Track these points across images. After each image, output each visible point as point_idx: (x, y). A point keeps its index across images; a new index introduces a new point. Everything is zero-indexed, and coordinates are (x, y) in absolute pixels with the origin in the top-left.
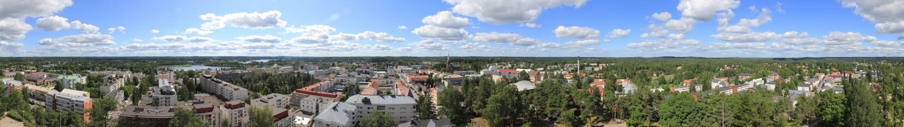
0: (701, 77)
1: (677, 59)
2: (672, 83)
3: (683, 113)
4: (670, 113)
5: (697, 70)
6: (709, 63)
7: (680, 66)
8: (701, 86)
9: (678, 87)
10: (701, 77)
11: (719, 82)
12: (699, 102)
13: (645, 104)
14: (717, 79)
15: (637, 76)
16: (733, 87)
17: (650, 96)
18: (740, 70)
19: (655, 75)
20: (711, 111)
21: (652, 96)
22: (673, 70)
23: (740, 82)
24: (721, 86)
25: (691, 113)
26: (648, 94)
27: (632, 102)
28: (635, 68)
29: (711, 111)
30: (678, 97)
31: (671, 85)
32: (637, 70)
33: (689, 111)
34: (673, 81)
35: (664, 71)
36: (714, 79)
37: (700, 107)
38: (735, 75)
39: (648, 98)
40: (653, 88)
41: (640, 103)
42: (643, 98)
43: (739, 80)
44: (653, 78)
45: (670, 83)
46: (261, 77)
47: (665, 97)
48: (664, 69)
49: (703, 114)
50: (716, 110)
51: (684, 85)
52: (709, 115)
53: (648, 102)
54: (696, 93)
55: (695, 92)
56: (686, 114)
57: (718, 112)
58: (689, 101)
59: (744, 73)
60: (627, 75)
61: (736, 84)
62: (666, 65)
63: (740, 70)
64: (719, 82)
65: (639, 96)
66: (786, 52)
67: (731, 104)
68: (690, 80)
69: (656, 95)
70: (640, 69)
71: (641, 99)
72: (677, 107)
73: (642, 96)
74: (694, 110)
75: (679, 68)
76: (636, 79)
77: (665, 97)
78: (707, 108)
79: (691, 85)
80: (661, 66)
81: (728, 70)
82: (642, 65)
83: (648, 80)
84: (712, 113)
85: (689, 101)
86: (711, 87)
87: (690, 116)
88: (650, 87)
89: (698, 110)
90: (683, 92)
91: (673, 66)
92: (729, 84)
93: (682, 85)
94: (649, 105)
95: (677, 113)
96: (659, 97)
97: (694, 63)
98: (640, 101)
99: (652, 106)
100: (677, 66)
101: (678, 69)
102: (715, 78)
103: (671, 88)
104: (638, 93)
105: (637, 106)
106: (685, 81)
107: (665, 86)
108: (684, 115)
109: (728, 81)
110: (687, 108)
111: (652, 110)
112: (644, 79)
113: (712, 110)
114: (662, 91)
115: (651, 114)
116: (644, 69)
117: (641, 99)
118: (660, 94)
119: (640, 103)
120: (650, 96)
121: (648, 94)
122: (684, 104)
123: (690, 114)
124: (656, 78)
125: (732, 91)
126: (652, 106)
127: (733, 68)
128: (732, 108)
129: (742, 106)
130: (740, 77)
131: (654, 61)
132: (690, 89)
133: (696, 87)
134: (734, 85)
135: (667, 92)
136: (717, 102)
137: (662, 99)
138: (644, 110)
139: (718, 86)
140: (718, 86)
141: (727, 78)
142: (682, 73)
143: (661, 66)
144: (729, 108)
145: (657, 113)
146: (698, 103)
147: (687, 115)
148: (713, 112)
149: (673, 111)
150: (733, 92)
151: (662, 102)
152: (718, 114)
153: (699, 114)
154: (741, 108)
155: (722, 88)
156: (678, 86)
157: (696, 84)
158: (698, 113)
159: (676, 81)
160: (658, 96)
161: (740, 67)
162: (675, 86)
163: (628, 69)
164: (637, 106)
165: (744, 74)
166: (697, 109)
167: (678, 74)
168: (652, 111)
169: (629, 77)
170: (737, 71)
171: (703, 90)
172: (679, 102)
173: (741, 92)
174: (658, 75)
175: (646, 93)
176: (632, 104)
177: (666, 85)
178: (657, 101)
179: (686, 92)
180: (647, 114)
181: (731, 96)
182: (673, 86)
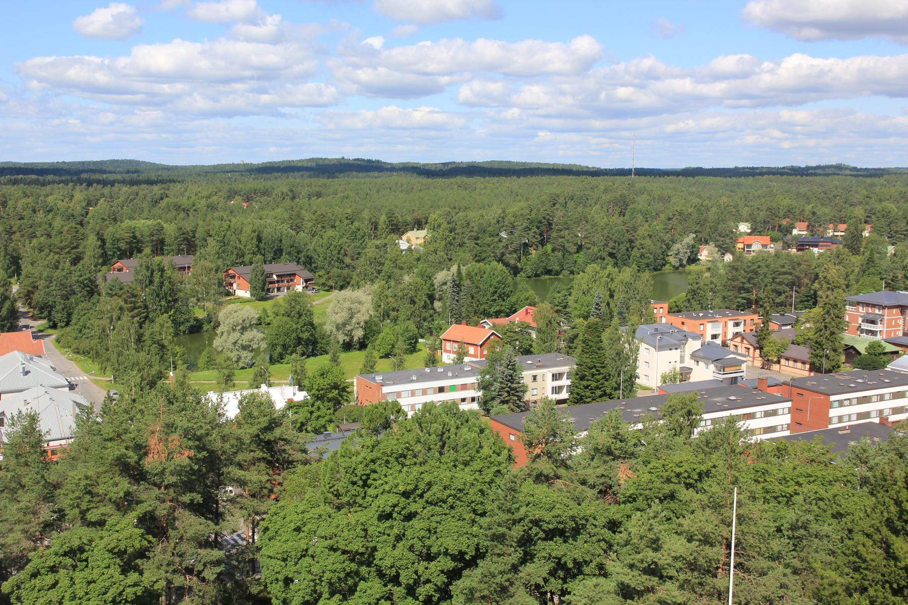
0: (562, 309)
1: (395, 178)
2: (363, 346)
3: (429, 557)
4: (334, 564)
5: (534, 253)
6: (622, 205)
7: (419, 224)
8: (565, 369)
9: (400, 374)
10: (562, 309)
11: (693, 345)
12: (540, 478)
13: (162, 511)
14: (677, 320)
15: (107, 303)
16: (793, 389)
17: (200, 443)
18: (857, 261)
19: (243, 293)
20: (650, 555)
21: (216, 444)
22: (371, 251)
23: (851, 352)
24: (703, 373)
25: (480, 555)
26: (186, 433)
27: (64, 502)
28: (92, 241)
29: (650, 555)
30: (390, 442)
31: (357, 358)
32: (106, 260)
33: (466, 545)
34: (370, 330)
35: (309, 262)
36: (650, 319)
37: (537, 514)
38: (812, 300)
39: (183, 459)
40: (228, 382)
41: (126, 503)
42: (150, 463)
43: (848, 338)
44: (229, 314)
45: (348, 346)
46: (144, 295)
47: (314, 445)
48: (313, 246)
49: (560, 565)
50: (676, 546)
51: (447, 358)
52: (635, 580)
53: (188, 487)
54: (524, 420)
55: (524, 407)
56: (450, 565)
57: (693, 566)
58: (464, 476)
59: (892, 286)
60: (28, 296)
61: (814, 368)
62: (324, 222)
63: (857, 261)
64: (693, 345)
65: (115, 450)
66: (869, 180)
67: (790, 515)
68: (488, 323)
69: (248, 432)
70: (133, 248)
71: (137, 475)
72: (385, 516)
73: (142, 449)
74: (499, 538)
75: (414, 239)
76: (97, 323)
77: (314, 445)
78: (613, 526)
79: (493, 360)
80: (285, 228)
81: (762, 259)
82: (143, 225)
83: (196, 329)
84: (653, 570)
85: (464, 476)
86: (632, 378)
87: (470, 579)
88: (200, 378)
89: (526, 541)
90: (428, 408)
91: (365, 227)
92: (767, 363)
93: (432, 361)
94: (195, 508)
95: (386, 557)
96: (269, 445)
97: (515, 208)
98: (125, 484)
99: (217, 517)
100: (398, 229)
101: (403, 245)
102: (660, 310)
103: (355, 383)
104: (108, 431)
105: (101, 523)
106: (455, 331)
107: (314, 364)
108: (435, 571)
109: (760, 340)
110: (452, 524)
111: (216, 544)
112: (162, 326)
113: (655, 545)
114: (291, 405)
115: (210, 574)
116: (159, 247)
117: (137, 475)
118: (273, 424)
119: (126, 503)
120: (200, 443)
121: (186, 433)
122: (436, 492)
123: (472, 563)
124: (252, 311)
125: (785, 419)
126: (217, 517)
127: (802, 246)
128: (797, 543)
129: (887, 547)
130: (854, 314)
131: (232, 194)
132: (484, 386)
133: (526, 376)
134: (801, 371)
135: (325, 409)
136: (685, 494)
137: (289, 464)
138: (160, 552)
139: (685, 373)
140: (685, 373)
141: (750, 321)
142: (428, 278)
143: (285, 228)
144: (776, 545)
145: (254, 566)
146: (528, 487)
147: (454, 575)
148: (662, 558)
149: (357, 546)
150: (796, 423)
151: (292, 479)
152: (694, 577)
153: (536, 570)
154: (874, 554)
155: (710, 390)
156: (400, 365)
157: (527, 352)
158: (527, 558)
159: (387, 332)
160: (257, 440)
161: (853, 243)
162: (383, 365)
163: (27, 250)
164: (101, 523)
165: (884, 296)
166: (517, 532)
167: (407, 278)
168: (217, 554)
169: (44, 310)
170: (834, 272)
171: (578, 399)
172: (402, 479)
173: (857, 431)
174: (262, 291)
175: (170, 427)
176: (61, 514)
177: (318, 363)
178: (256, 476)
179: (451, 408)
180: (178, 581)
181: (780, 450)
182: (369, 369)
